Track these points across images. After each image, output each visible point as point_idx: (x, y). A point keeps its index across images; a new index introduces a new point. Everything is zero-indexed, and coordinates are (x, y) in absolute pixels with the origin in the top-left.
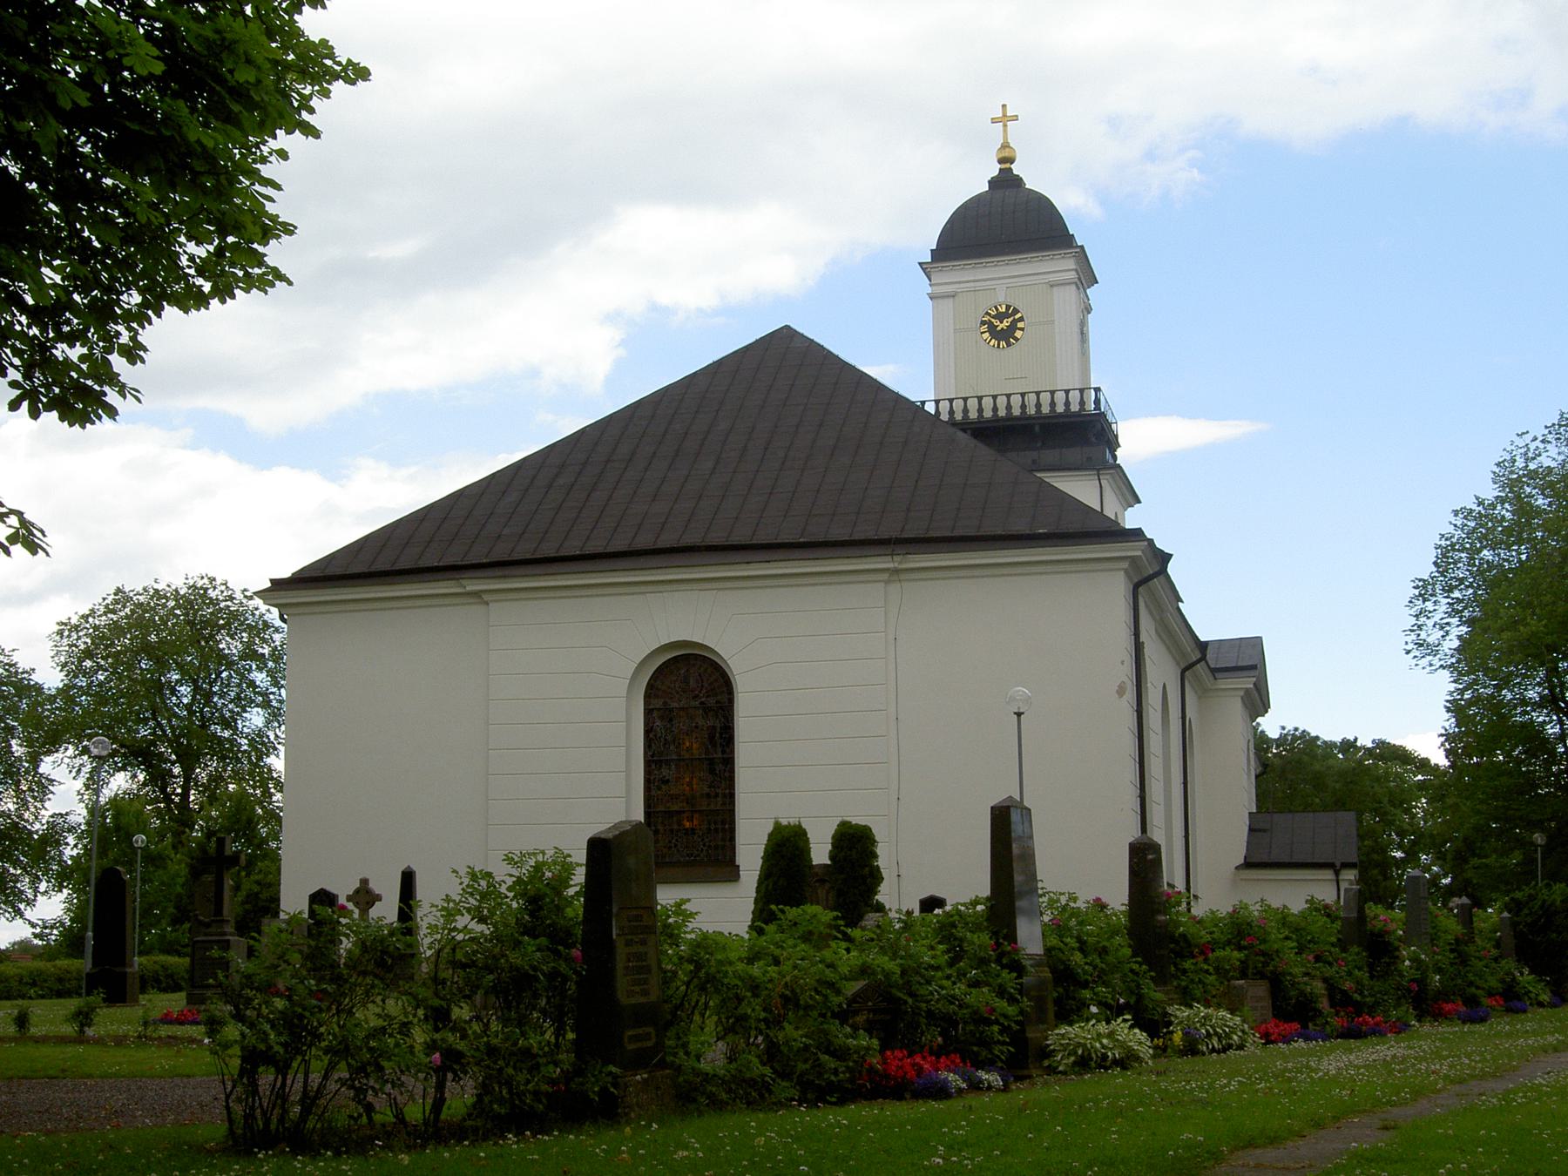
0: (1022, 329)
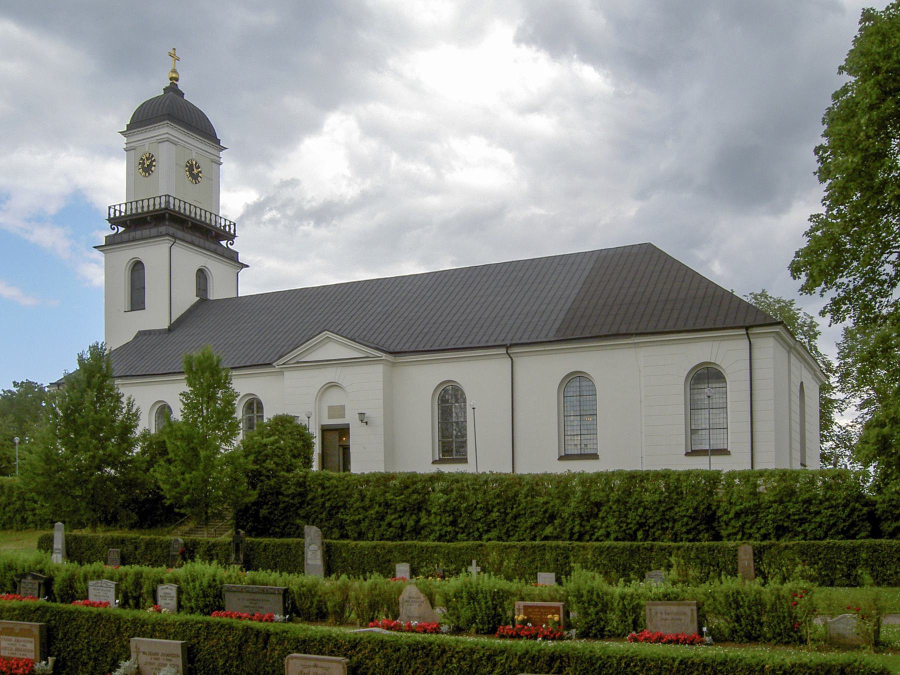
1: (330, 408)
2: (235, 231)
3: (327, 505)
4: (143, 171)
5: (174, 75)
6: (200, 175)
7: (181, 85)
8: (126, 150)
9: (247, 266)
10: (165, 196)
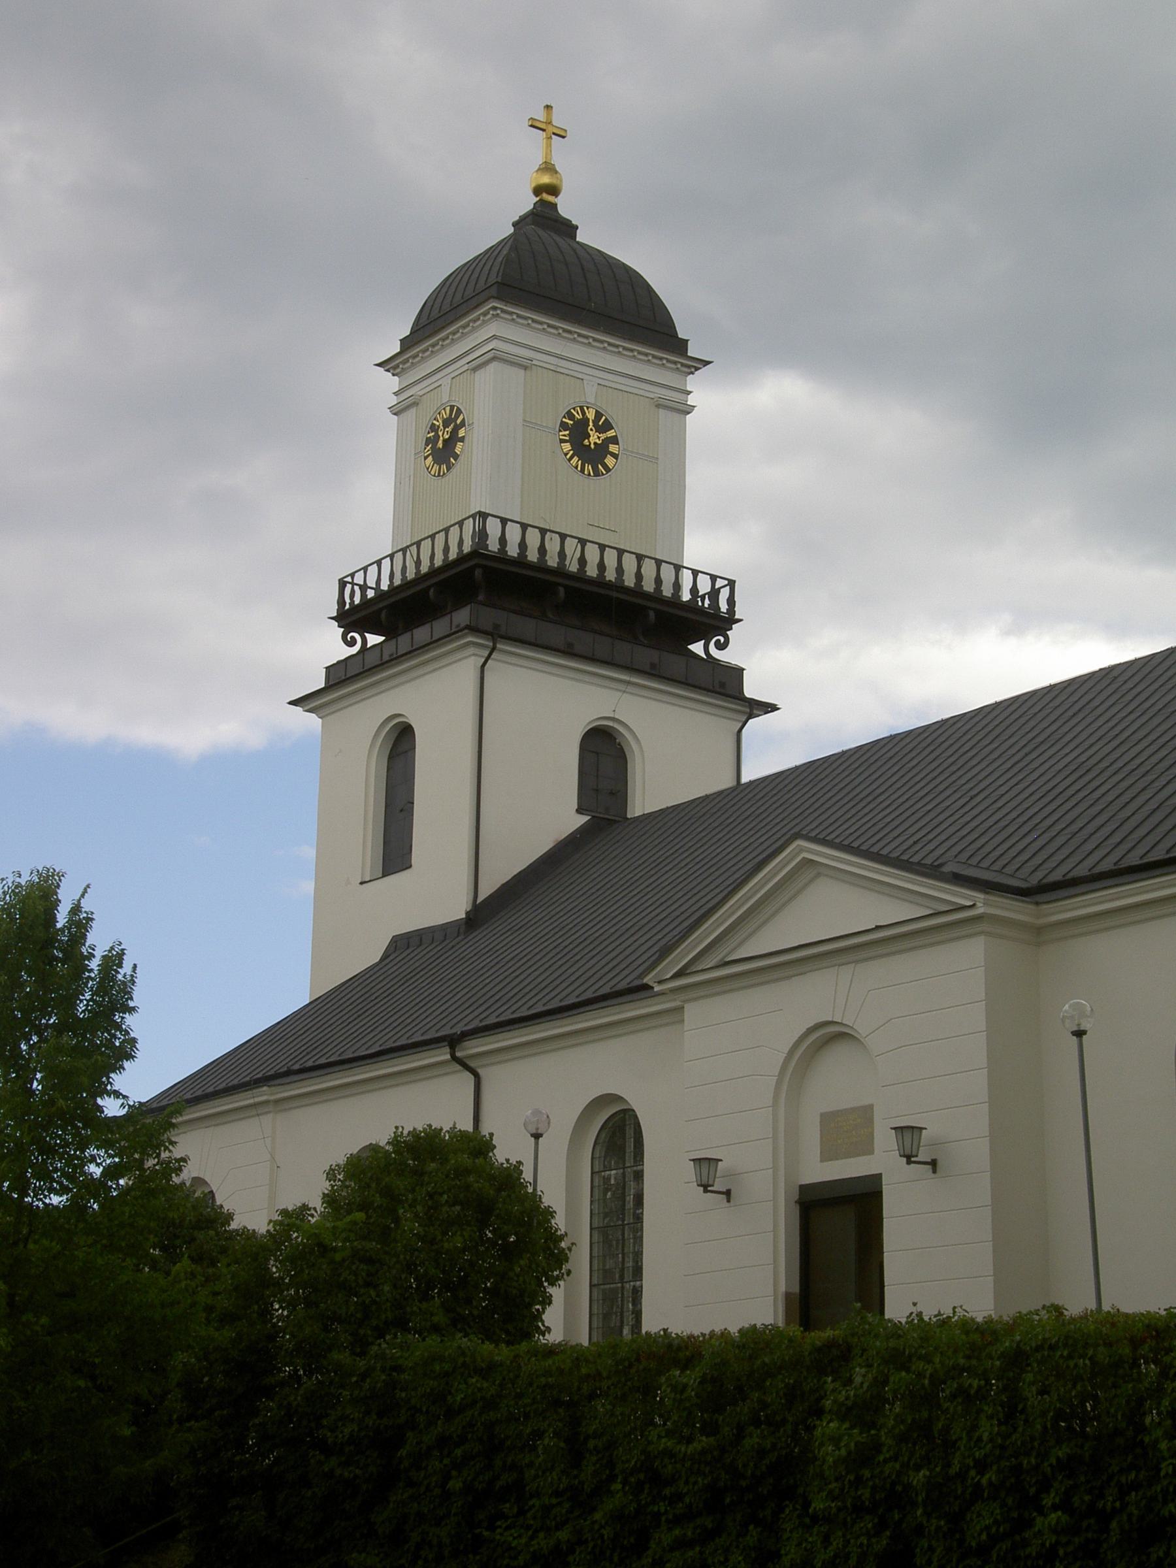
0: (615, 456)
1: (827, 1119)
2: (731, 601)
3: (455, 1484)
4: (436, 461)
5: (546, 179)
6: (613, 448)
7: (566, 207)
8: (397, 411)
9: (771, 708)
10: (473, 516)
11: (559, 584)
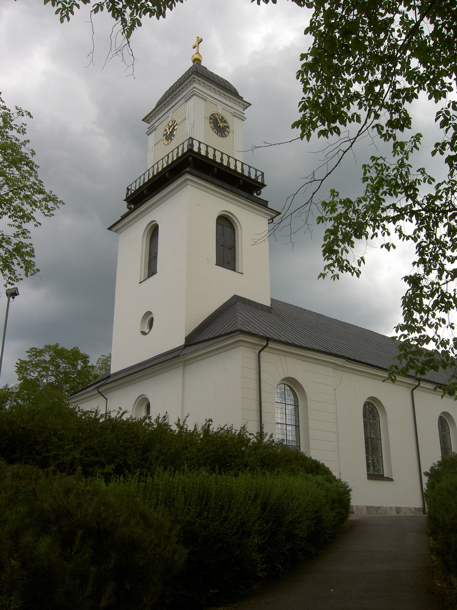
5: (197, 56)
11: (216, 167)
